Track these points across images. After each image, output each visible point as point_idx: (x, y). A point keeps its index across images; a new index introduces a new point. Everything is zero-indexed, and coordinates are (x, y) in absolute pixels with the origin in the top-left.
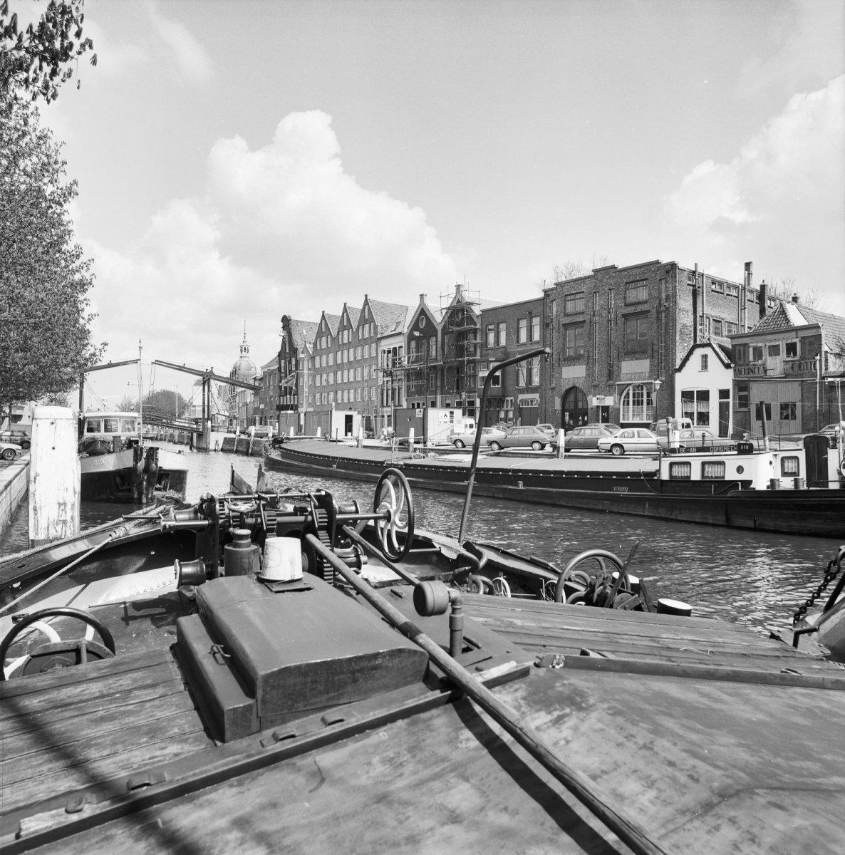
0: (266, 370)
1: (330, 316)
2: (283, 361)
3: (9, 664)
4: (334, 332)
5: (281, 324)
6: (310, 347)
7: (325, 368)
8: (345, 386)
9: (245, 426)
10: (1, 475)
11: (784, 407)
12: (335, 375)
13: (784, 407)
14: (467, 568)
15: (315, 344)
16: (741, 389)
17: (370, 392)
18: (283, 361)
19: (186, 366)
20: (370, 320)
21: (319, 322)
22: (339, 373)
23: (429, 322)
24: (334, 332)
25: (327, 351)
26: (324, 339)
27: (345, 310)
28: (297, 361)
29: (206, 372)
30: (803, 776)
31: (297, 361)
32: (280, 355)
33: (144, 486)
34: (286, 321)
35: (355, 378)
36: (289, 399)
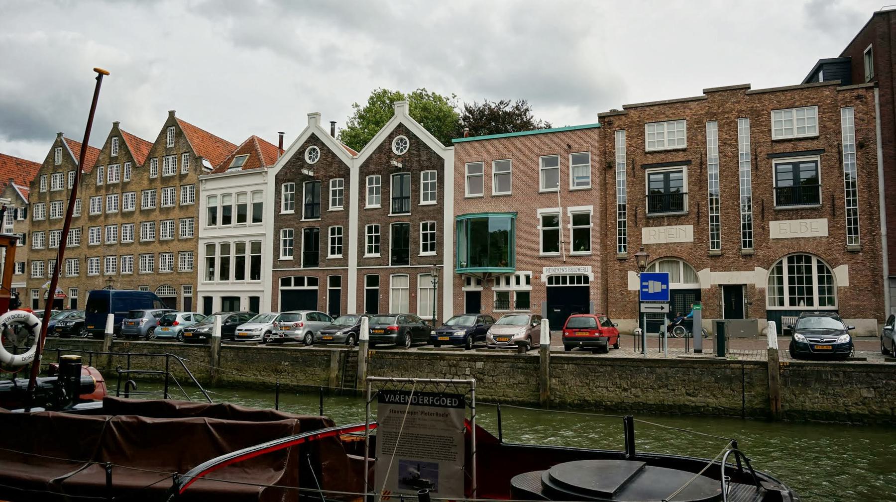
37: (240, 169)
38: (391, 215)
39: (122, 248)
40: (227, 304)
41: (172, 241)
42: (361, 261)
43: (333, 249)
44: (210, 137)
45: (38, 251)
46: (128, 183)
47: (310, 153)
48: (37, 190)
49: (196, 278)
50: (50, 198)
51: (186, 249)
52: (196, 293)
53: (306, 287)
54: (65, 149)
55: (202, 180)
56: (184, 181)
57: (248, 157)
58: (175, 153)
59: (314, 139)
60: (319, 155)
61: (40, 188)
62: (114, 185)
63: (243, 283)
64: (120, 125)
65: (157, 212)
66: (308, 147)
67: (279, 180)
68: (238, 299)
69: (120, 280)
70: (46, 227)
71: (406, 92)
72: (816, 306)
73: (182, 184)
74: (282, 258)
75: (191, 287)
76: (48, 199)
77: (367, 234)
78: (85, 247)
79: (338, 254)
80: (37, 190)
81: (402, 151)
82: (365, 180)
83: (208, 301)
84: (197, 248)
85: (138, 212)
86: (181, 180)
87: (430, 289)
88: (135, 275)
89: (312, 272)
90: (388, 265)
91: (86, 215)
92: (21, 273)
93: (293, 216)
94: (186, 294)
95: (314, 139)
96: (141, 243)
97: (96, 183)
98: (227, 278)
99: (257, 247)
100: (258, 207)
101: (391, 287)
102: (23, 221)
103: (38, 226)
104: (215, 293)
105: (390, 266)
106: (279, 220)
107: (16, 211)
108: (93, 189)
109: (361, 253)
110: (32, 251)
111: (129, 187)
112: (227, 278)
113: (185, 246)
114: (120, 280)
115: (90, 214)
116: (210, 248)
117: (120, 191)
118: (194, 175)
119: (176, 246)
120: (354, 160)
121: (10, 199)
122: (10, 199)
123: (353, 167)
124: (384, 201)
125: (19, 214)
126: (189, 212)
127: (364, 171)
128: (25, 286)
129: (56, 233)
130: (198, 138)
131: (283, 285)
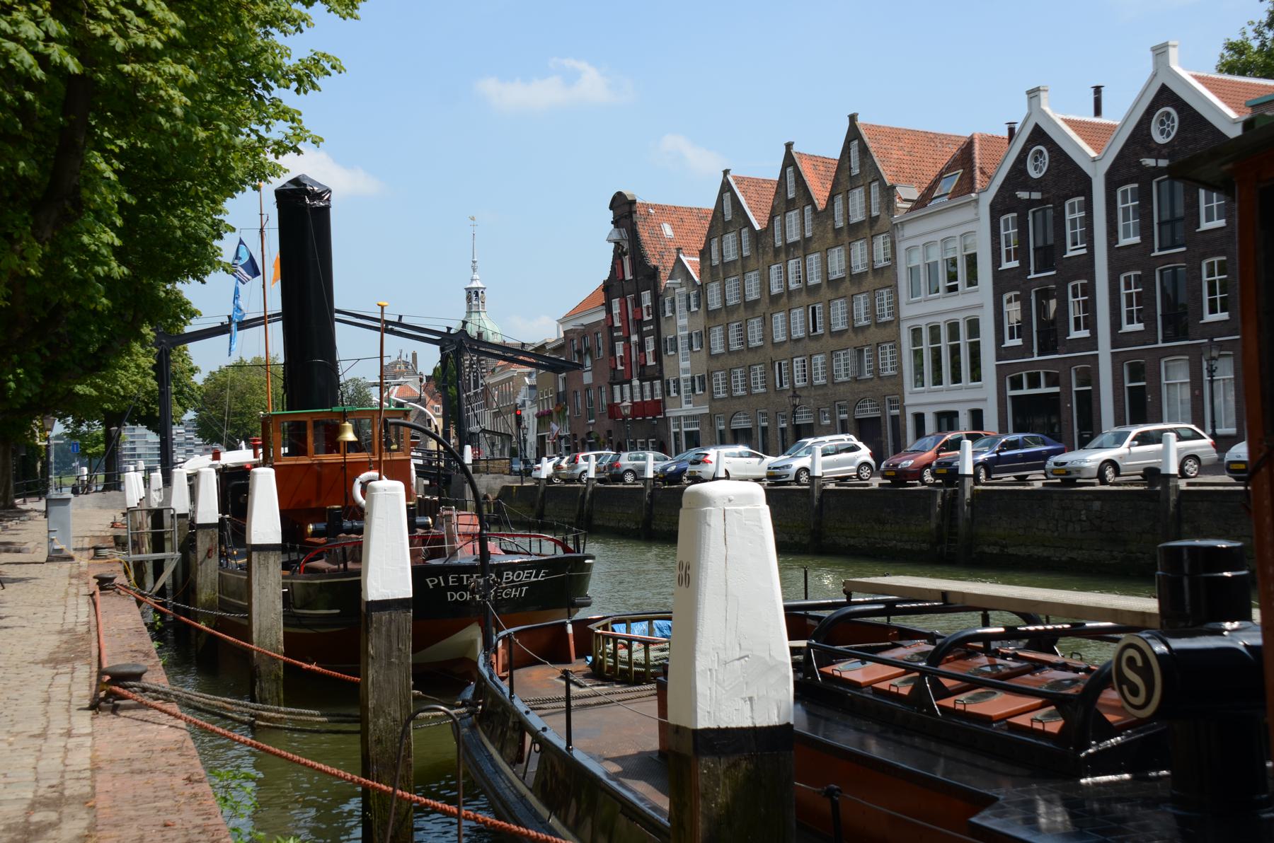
0: (569, 327)
1: (877, 130)
2: (616, 304)
3: (73, 71)
4: (820, 195)
5: (610, 214)
6: (691, 262)
7: (736, 307)
8: (734, 361)
9: (276, 463)
10: (7, 547)
11: (940, 416)
12: (766, 322)
13: (940, 416)
14: (836, 787)
15: (704, 254)
16: (1136, 373)
17: (747, 377)
18: (616, 304)
19: (404, 321)
20: (871, 172)
21: (835, 153)
22: (779, 318)
23: (1062, 162)
24: (820, 195)
25: (743, 265)
26: (857, 196)
27: (789, 160)
28: (656, 298)
29: (448, 333)
30: (546, 768)
31: (656, 298)
32: (608, 288)
33: (39, 469)
34: (623, 208)
35: (727, 345)
36: (637, 390)
37: (945, 199)
38: (1156, 253)
39: (812, 344)
40: (944, 421)
41: (868, 326)
42: (1118, 339)
43: (1212, 303)
44: (932, 140)
45: (718, 356)
46: (810, 239)
47: (1162, 123)
48: (708, 263)
49: (901, 385)
50: (724, 273)
51: (887, 339)
52: (903, 409)
53: (1043, 390)
54: (734, 195)
55: (896, 224)
56: (876, 228)
57: (959, 175)
58: (861, 183)
59: (1165, 96)
60: (1176, 124)
61: (711, 260)
62: (795, 244)
63: (961, 389)
64: (117, 492)
65: (847, 283)
66: (1031, 149)
67: (997, 210)
68: (956, 414)
69: (813, 394)
70: (723, 317)
71: (81, 496)
72: (1011, 393)
73: (873, 233)
74: (1126, 328)
75: (899, 403)
76: (721, 275)
77: (1123, 291)
78: (769, 345)
79: (1222, 311)
80: (708, 263)
81: (1168, 135)
82: (1116, 196)
83: (919, 418)
84: (898, 335)
85: (825, 285)
86: (871, 227)
87: (1181, 383)
88: (829, 385)
89: (772, 378)
90: (1157, 343)
91: (767, 296)
92: (702, 392)
93: (1141, 246)
94: (892, 411)
95: (1165, 96)
96: (877, 325)
97: (774, 243)
98: (940, 383)
99: (974, 326)
100: (972, 261)
101: (1164, 381)
102: (671, 317)
103: (715, 318)
104: (962, 404)
105: (1160, 345)
106: (1002, 282)
107: (688, 298)
108: (771, 254)
109: (1115, 324)
110: (711, 356)
111: (815, 245)
112: (940, 383)
113: (886, 333)
114: (813, 394)
115: (809, 284)
116: (916, 332)
117: (801, 253)
118: (887, 216)
119: (875, 335)
120: (1098, 163)
121: (679, 281)
122: (679, 281)
123: (1096, 176)
124: (1145, 230)
125: (693, 304)
126: (883, 276)
127: (1114, 179)
128: (707, 411)
129: (885, 294)
130: (901, 148)
131: (1013, 388)
